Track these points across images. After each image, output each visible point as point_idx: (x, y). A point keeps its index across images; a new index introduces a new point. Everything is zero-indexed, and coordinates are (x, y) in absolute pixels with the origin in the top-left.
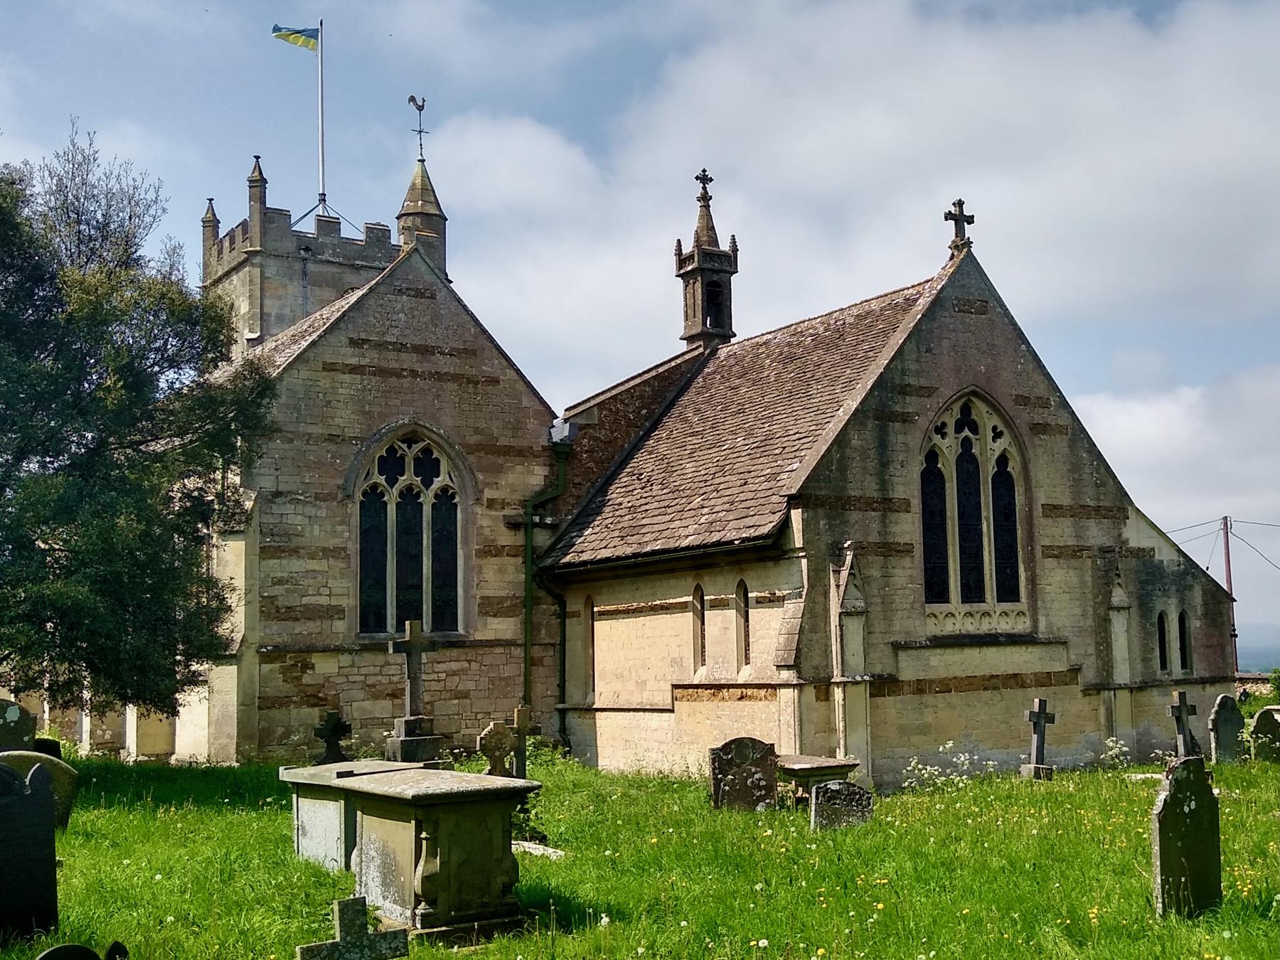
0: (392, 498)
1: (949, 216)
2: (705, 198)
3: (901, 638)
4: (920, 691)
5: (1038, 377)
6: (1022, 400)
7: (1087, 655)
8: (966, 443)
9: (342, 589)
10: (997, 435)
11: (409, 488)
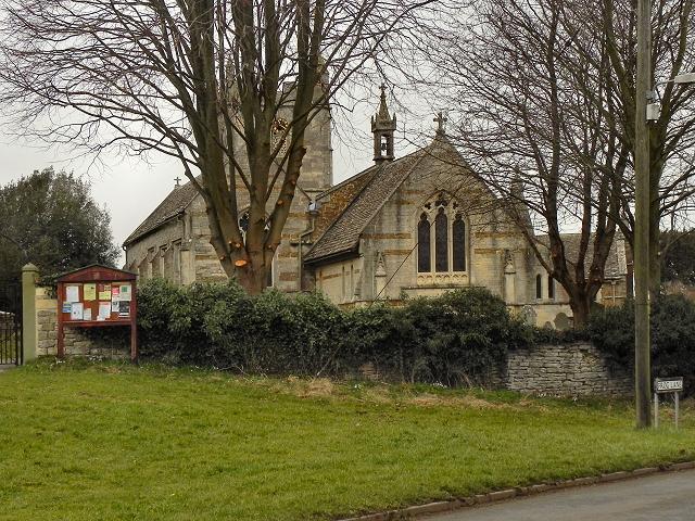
3: (405, 285)
8: (441, 210)
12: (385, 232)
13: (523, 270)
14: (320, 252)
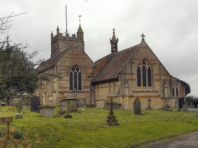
0: (73, 73)
1: (141, 36)
2: (114, 32)
5: (154, 57)
7: (161, 94)
9: (68, 85)
10: (148, 64)
11: (76, 72)
12: (127, 72)
13: (169, 87)
14: (98, 79)
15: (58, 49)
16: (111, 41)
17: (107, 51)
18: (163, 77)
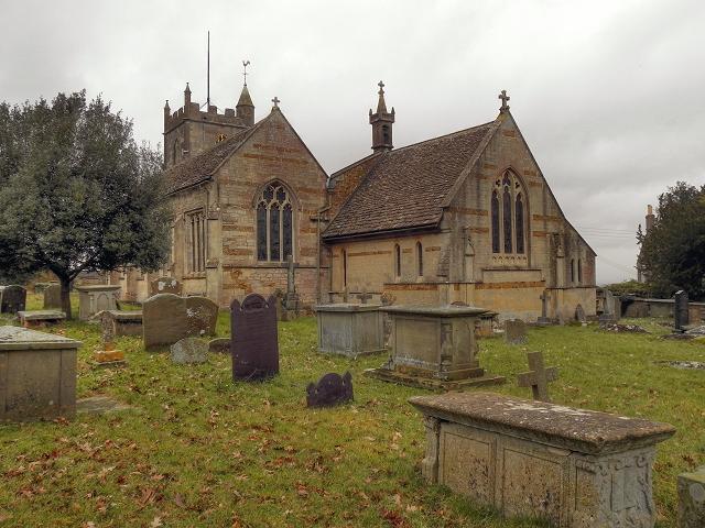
0: (269, 207)
2: (381, 93)
4: (491, 287)
6: (526, 172)
10: (518, 186)
11: (275, 204)
12: (468, 207)
15: (186, 145)
16: (372, 117)
17: (361, 145)
18: (551, 228)
